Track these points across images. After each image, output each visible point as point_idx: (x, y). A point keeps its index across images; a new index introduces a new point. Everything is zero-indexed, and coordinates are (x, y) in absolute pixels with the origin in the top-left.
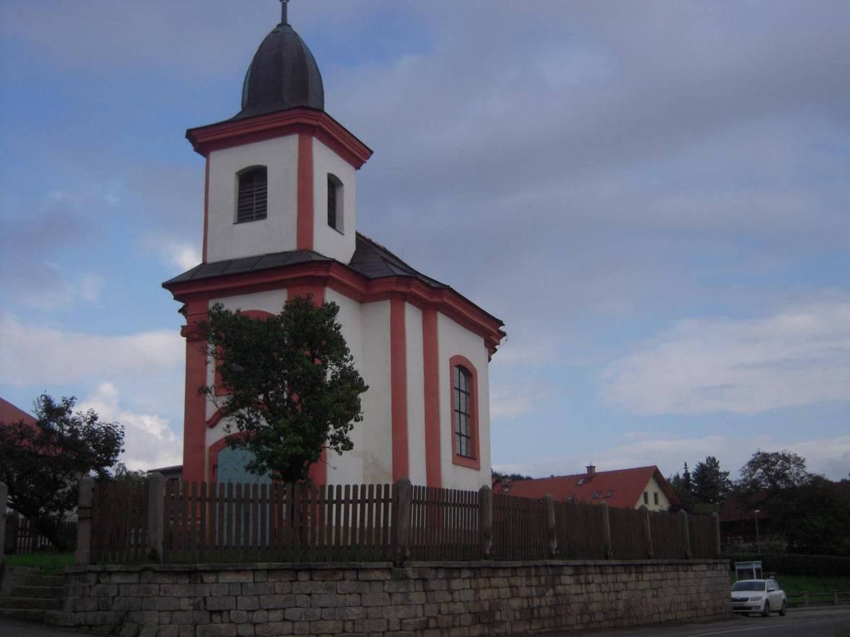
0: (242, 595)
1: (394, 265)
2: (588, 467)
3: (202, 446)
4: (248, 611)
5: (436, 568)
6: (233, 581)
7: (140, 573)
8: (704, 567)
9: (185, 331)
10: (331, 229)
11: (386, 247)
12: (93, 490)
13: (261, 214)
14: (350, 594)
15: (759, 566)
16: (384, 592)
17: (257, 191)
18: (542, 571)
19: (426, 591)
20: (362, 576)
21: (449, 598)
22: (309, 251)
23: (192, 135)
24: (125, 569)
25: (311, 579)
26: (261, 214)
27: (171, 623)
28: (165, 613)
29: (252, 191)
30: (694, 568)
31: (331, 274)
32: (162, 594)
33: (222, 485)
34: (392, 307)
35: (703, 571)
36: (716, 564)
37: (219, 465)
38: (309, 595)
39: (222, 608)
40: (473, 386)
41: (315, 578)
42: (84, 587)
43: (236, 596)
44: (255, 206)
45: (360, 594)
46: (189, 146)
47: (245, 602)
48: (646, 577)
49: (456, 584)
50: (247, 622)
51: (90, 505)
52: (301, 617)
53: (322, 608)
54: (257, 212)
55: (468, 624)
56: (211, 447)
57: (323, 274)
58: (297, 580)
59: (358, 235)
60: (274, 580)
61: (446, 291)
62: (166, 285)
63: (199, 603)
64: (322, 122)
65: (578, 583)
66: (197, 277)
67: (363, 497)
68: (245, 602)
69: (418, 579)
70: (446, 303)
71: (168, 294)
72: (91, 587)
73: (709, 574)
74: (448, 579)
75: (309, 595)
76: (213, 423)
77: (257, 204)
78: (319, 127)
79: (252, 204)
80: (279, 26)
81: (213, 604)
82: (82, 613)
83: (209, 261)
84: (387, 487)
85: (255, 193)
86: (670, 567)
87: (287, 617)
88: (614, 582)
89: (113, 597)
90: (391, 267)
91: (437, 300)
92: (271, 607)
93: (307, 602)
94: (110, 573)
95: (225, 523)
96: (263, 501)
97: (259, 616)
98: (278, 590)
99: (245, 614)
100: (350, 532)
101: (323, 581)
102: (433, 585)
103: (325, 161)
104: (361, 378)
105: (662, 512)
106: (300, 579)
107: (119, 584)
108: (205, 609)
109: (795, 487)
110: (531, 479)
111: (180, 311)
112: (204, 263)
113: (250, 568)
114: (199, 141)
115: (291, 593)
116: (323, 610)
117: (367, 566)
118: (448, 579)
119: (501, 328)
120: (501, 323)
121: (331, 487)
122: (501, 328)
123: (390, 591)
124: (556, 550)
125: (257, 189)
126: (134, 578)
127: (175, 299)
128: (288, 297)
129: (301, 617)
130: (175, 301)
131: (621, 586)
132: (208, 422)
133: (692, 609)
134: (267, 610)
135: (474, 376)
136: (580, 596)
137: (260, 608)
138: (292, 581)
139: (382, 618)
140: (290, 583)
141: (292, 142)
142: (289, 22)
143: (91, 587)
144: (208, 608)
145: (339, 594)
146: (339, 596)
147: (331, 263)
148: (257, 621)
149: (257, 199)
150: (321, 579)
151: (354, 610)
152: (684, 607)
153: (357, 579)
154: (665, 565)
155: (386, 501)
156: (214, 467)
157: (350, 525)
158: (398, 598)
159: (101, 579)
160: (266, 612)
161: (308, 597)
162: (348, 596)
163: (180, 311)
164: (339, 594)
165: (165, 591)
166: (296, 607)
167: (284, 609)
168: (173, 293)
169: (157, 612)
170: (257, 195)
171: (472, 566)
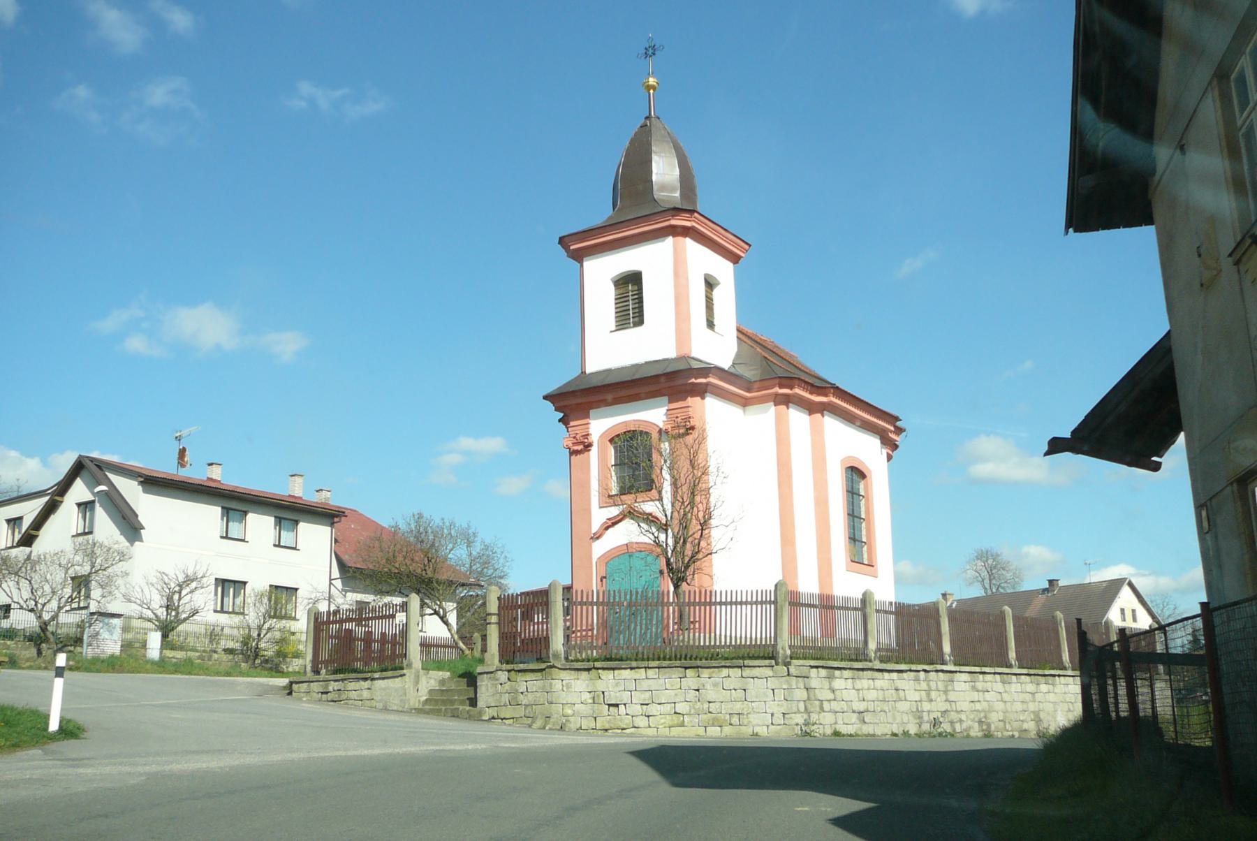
0: (636, 690)
10: (709, 331)
11: (778, 343)
16: (767, 688)
20: (747, 672)
21: (831, 696)
22: (688, 357)
38: (698, 690)
43: (636, 690)
45: (745, 690)
47: (639, 697)
49: (838, 684)
52: (690, 711)
53: (709, 702)
59: (1046, 454)
60: (664, 677)
62: (545, 398)
65: (974, 689)
66: (565, 391)
71: (549, 405)
74: (830, 678)
75: (698, 690)
76: (597, 537)
82: (990, 683)
87: (677, 711)
95: (527, 628)
97: (653, 709)
98: (668, 686)
99: (639, 706)
101: (709, 678)
111: (560, 421)
113: (643, 666)
114: (572, 248)
116: (711, 704)
119: (898, 424)
120: (897, 419)
122: (898, 424)
127: (556, 410)
129: (690, 711)
130: (1078, 234)
136: (832, 702)
137: (653, 702)
146: (724, 691)
147: (707, 370)
150: (707, 676)
158: (780, 695)
161: (697, 692)
163: (560, 421)
167: (675, 703)
168: (554, 405)
169: (561, 705)
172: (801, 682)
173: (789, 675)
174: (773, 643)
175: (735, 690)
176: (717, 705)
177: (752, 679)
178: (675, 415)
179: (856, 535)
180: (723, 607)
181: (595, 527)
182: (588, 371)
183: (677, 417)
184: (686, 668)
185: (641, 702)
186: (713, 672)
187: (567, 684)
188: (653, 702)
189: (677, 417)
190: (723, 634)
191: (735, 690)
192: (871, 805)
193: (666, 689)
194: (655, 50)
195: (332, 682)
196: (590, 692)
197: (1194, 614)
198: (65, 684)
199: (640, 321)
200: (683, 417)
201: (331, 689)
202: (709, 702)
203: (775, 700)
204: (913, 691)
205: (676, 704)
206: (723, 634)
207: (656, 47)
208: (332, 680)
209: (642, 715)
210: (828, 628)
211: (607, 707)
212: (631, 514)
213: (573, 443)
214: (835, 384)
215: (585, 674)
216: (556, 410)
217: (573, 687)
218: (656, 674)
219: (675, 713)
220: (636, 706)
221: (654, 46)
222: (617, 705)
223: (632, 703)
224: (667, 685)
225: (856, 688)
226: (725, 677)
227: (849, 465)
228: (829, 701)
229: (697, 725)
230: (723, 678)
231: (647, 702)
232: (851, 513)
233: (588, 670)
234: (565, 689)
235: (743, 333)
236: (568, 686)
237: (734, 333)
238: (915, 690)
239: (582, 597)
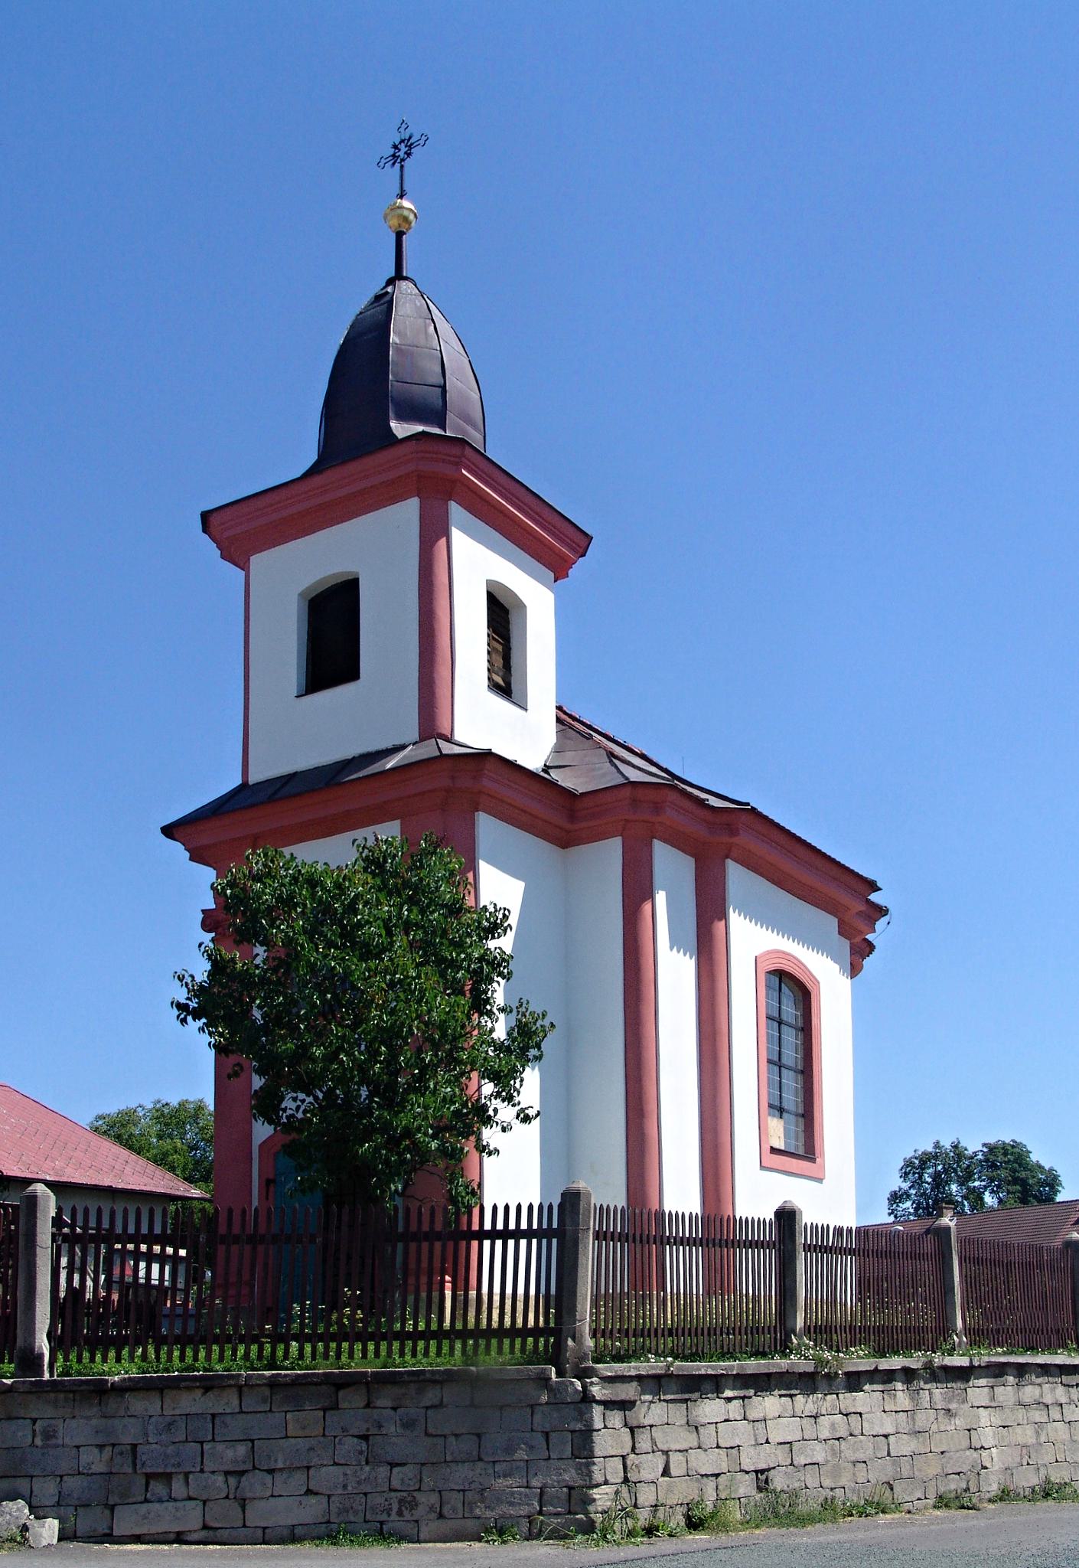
0: (213, 1440)
4: (227, 1473)
9: (207, 923)
13: (351, 673)
32: (38, 1442)
34: (248, 781)
41: (379, 1403)
45: (479, 1436)
55: (787, 1464)
58: (335, 1407)
81: (152, 1457)
92: (280, 1465)
93: (361, 1452)
97: (255, 1485)
105: (387, 1343)
109: (211, 1287)
110: (561, 1203)
119: (874, 897)
120: (873, 886)
122: (874, 897)
127: (191, 859)
172: (616, 1418)
173: (532, 1430)
174: (552, 1325)
175: (456, 1435)
176: (409, 1471)
179: (784, 1101)
180: (425, 1245)
182: (251, 782)
185: (226, 1468)
188: (254, 1468)
190: (509, 1290)
191: (456, 1435)
199: (351, 673)
202: (393, 1465)
203: (549, 1458)
204: (879, 1414)
206: (509, 1290)
207: (412, 141)
209: (227, 1497)
210: (718, 1280)
214: (748, 804)
216: (191, 859)
217: (60, 1434)
218: (264, 1401)
220: (213, 1477)
221: (410, 138)
224: (290, 1427)
225: (751, 1418)
227: (773, 967)
230: (427, 1408)
231: (242, 1468)
232: (776, 1058)
234: (38, 1442)
235: (565, 713)
236: (48, 1435)
237: (553, 713)
239: (432, 1222)
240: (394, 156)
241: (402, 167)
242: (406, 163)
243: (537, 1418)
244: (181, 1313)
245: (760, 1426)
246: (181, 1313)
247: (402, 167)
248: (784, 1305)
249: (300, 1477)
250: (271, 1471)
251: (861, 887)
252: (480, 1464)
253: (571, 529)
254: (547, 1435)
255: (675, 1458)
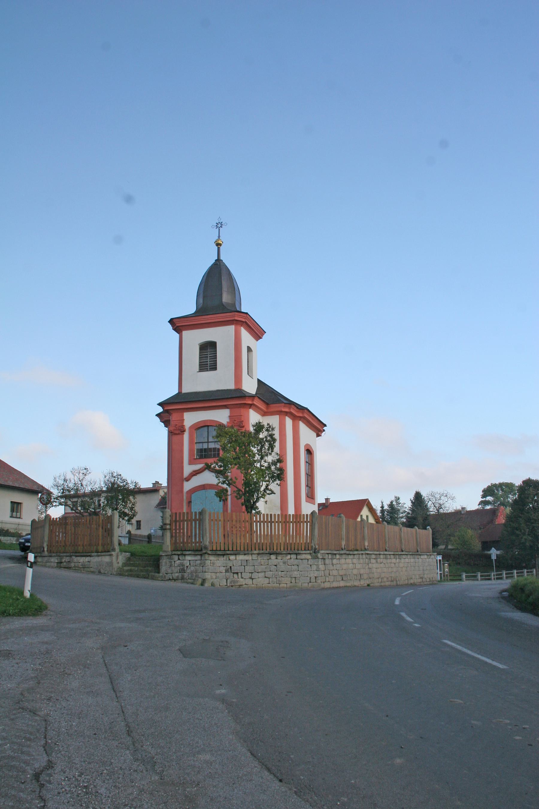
1: (278, 395)
2: (325, 499)
3: (182, 491)
5: (328, 554)
6: (243, 559)
7: (201, 555)
8: (426, 557)
12: (170, 516)
13: (214, 367)
14: (293, 565)
15: (441, 558)
17: (210, 354)
18: (364, 556)
19: (324, 564)
23: (172, 321)
24: (193, 553)
25: (277, 558)
26: (214, 367)
27: (216, 579)
28: (213, 573)
29: (207, 354)
30: (422, 557)
31: (255, 403)
32: (212, 565)
33: (304, 515)
35: (425, 559)
36: (431, 555)
37: (192, 501)
38: (276, 565)
39: (238, 572)
40: (312, 460)
41: (278, 558)
42: (171, 562)
43: (244, 566)
44: (209, 363)
45: (298, 565)
46: (170, 326)
47: (249, 569)
48: (403, 560)
50: (249, 578)
51: (169, 523)
52: (272, 576)
54: (210, 366)
56: (187, 492)
57: (250, 402)
59: (258, 379)
61: (306, 410)
63: (228, 569)
64: (247, 320)
67: (270, 520)
68: (249, 569)
69: (322, 559)
70: (306, 417)
72: (175, 562)
73: (427, 560)
75: (276, 565)
76: (188, 479)
77: (210, 361)
78: (246, 322)
79: (207, 362)
80: (216, 260)
81: (234, 569)
83: (184, 391)
84: (278, 515)
85: (209, 356)
86: (412, 556)
88: (390, 563)
89: (187, 567)
90: (278, 397)
91: (301, 415)
92: (260, 571)
94: (185, 555)
96: (195, 520)
97: (255, 575)
100: (262, 536)
101: (281, 559)
102: (327, 561)
103: (246, 337)
104: (482, 492)
106: (272, 558)
107: (190, 561)
108: (231, 572)
111: (157, 415)
112: (180, 393)
113: (250, 553)
115: (268, 565)
117: (301, 553)
118: (332, 559)
121: (304, 515)
123: (311, 564)
124: (367, 546)
125: (210, 353)
126: (198, 557)
128: (230, 414)
131: (393, 565)
132: (185, 479)
133: (421, 578)
134: (258, 573)
135: (313, 454)
138: (268, 559)
139: (307, 576)
140: (267, 560)
141: (231, 329)
142: (222, 258)
143: (175, 562)
144: (232, 572)
145: (289, 565)
146: (288, 566)
148: (253, 578)
149: (210, 359)
151: (296, 572)
152: (418, 577)
153: (297, 559)
154: (410, 555)
155: (307, 522)
156: (190, 502)
157: (262, 534)
159: (180, 558)
160: (257, 574)
162: (292, 566)
164: (289, 565)
165: (213, 563)
166: (270, 571)
167: (265, 572)
170: (210, 357)
171: (340, 553)
176: (285, 573)
177: (301, 560)
178: (234, 419)
181: (186, 473)
183: (235, 420)
184: (271, 554)
186: (283, 556)
187: (213, 563)
189: (235, 420)
192: (419, 626)
193: (261, 565)
194: (222, 225)
195: (65, 557)
196: (224, 567)
197: (209, 439)
198: (33, 572)
200: (238, 421)
201: (63, 560)
205: (266, 573)
207: (222, 223)
208: (65, 556)
211: (232, 574)
212: (208, 467)
213: (174, 430)
215: (222, 557)
217: (216, 563)
219: (265, 577)
221: (221, 223)
222: (237, 573)
223: (245, 572)
226: (289, 559)
228: (332, 570)
229: (276, 583)
233: (224, 555)
238: (359, 563)
240: (217, 226)
241: (219, 229)
242: (221, 229)
243: (309, 562)
244: (30, 532)
245: (359, 563)
246: (30, 532)
247: (219, 229)
248: (203, 538)
249: (263, 574)
250: (258, 573)
251: (323, 426)
252: (298, 572)
253: (250, 318)
254: (311, 565)
255: (331, 572)
